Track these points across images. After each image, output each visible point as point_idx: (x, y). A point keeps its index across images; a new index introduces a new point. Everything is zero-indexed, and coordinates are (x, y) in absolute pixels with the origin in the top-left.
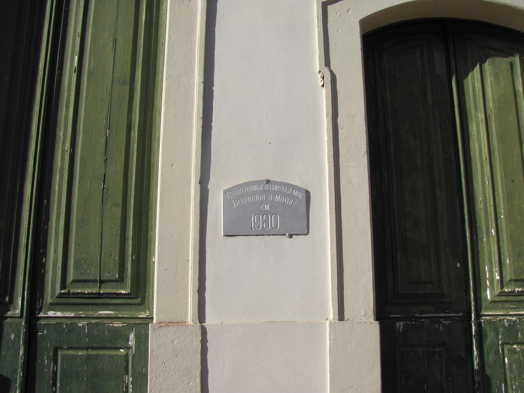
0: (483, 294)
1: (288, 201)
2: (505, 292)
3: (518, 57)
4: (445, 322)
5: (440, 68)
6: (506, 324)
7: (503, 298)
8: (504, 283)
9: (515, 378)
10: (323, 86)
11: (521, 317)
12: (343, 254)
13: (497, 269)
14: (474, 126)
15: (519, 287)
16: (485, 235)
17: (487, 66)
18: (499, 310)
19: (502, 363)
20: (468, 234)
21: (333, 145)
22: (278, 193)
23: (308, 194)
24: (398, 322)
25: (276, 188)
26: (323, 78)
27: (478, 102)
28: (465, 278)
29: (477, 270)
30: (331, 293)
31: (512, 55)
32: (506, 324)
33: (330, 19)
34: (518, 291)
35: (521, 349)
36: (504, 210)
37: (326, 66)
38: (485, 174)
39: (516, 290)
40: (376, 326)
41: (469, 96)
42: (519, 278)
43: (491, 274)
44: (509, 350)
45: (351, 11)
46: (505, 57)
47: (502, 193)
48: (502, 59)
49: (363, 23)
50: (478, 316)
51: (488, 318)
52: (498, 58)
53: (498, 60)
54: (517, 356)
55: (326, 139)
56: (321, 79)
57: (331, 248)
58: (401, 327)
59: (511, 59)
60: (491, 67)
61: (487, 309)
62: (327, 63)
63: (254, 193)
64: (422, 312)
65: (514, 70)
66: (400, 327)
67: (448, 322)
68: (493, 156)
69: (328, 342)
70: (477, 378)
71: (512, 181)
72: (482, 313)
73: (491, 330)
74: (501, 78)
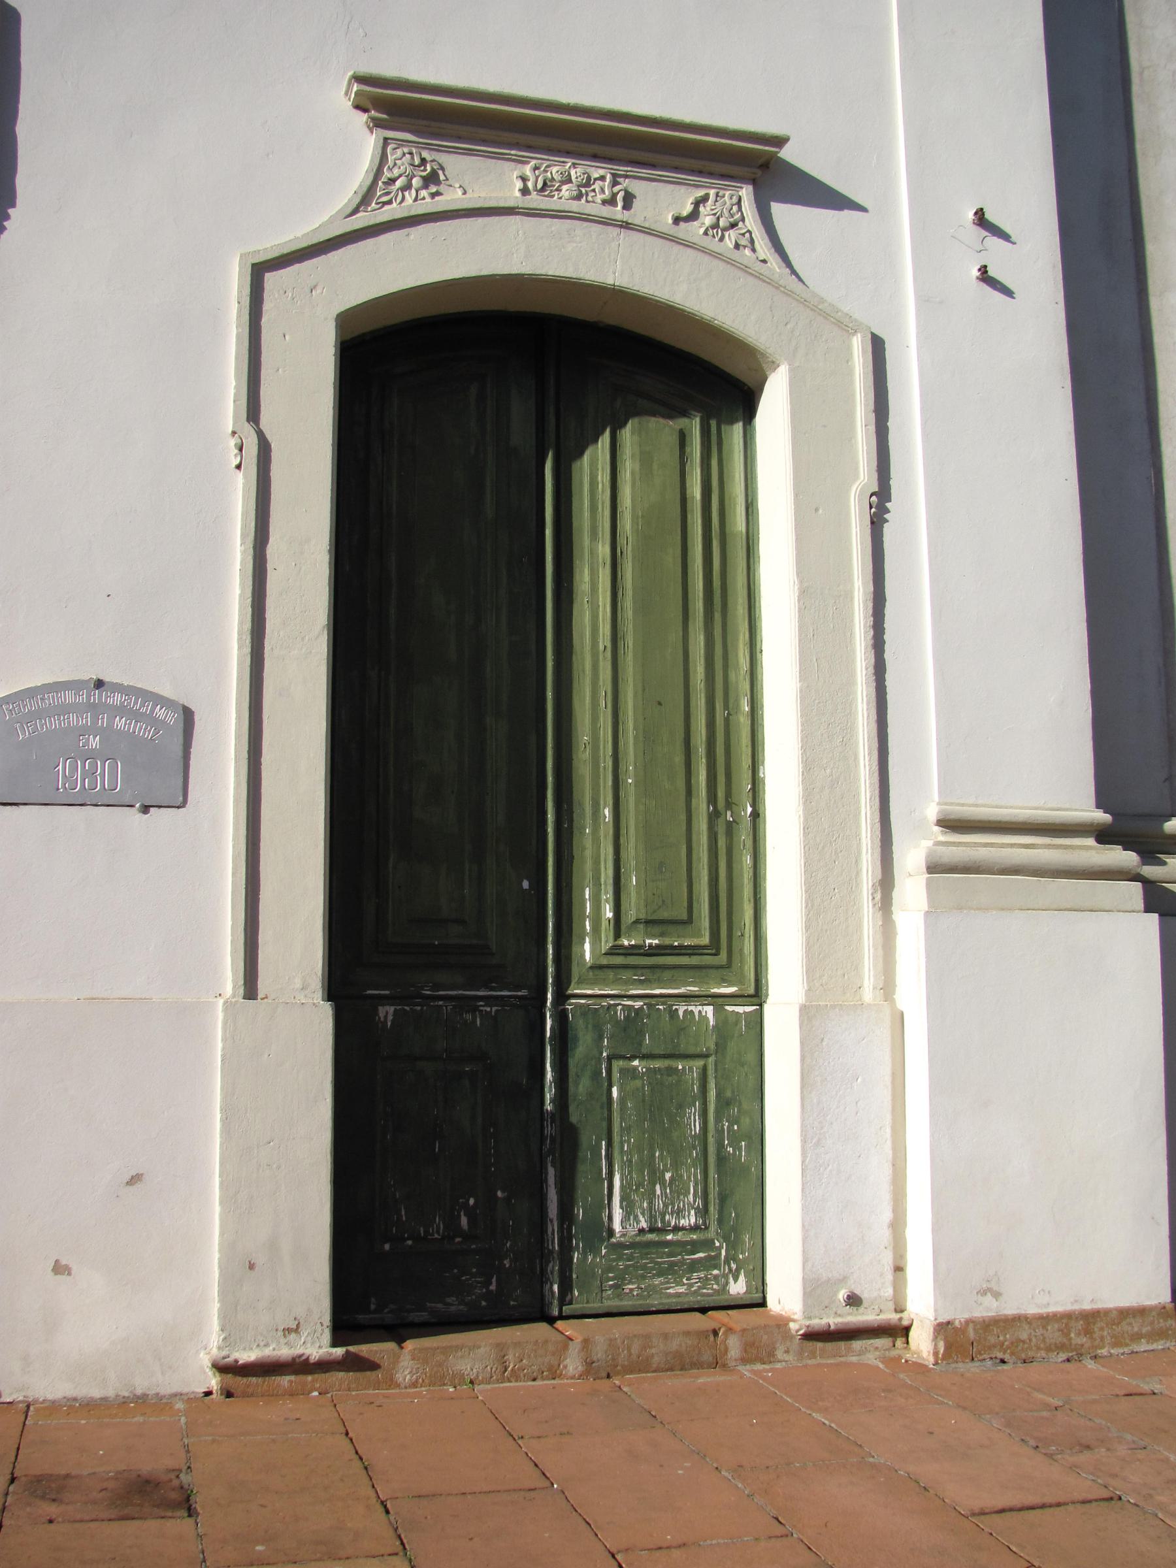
0: (575, 949)
1: (144, 731)
2: (622, 946)
3: (698, 419)
4: (488, 1009)
5: (521, 434)
6: (621, 1015)
7: (619, 960)
8: (623, 927)
9: (628, 1129)
10: (239, 467)
11: (653, 1001)
12: (262, 852)
13: (610, 895)
14: (586, 571)
15: (653, 936)
16: (588, 821)
17: (627, 434)
18: (607, 986)
19: (604, 1099)
20: (550, 817)
21: (253, 606)
22: (121, 711)
23: (188, 716)
24: (383, 1005)
25: (117, 699)
26: (241, 450)
27: (599, 516)
28: (536, 917)
29: (565, 899)
30: (230, 938)
31: (684, 413)
32: (621, 1015)
33: (267, 306)
34: (650, 945)
35: (648, 1069)
36: (635, 767)
37: (248, 421)
38: (601, 683)
39: (648, 941)
40: (326, 1012)
41: (582, 504)
42: (654, 917)
43: (595, 906)
44: (621, 1071)
45: (319, 291)
46: (670, 417)
47: (635, 729)
48: (661, 420)
49: (344, 320)
50: (562, 996)
51: (583, 1001)
52: (653, 419)
53: (654, 423)
54: (638, 1083)
55: (238, 591)
56: (236, 451)
57: (234, 840)
58: (390, 1018)
59: (682, 422)
60: (636, 438)
61: (581, 982)
62: (253, 412)
63: (65, 710)
64: (437, 987)
65: (688, 449)
66: (386, 1017)
67: (494, 1009)
68: (621, 644)
69: (220, 1045)
70: (548, 1131)
71: (660, 704)
72: (570, 992)
73: (587, 1027)
74: (655, 466)
